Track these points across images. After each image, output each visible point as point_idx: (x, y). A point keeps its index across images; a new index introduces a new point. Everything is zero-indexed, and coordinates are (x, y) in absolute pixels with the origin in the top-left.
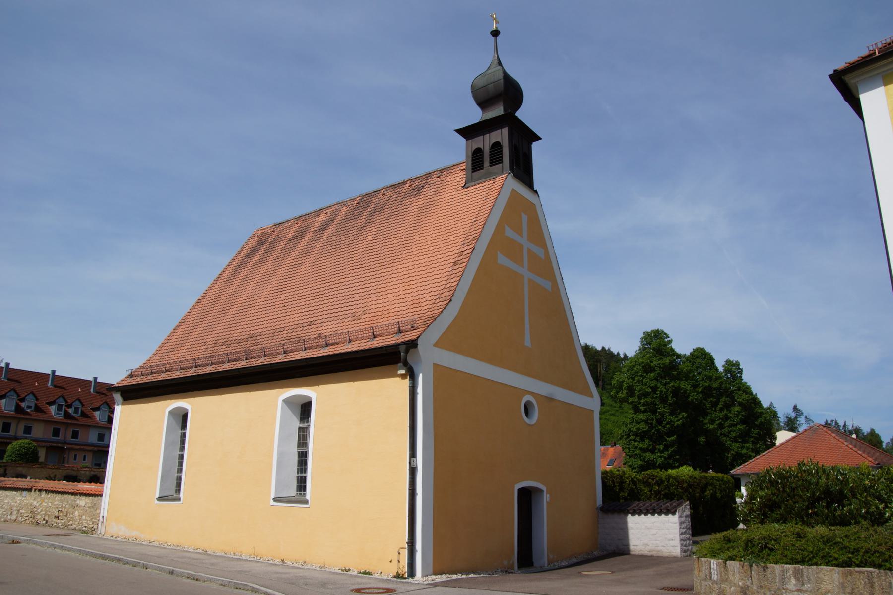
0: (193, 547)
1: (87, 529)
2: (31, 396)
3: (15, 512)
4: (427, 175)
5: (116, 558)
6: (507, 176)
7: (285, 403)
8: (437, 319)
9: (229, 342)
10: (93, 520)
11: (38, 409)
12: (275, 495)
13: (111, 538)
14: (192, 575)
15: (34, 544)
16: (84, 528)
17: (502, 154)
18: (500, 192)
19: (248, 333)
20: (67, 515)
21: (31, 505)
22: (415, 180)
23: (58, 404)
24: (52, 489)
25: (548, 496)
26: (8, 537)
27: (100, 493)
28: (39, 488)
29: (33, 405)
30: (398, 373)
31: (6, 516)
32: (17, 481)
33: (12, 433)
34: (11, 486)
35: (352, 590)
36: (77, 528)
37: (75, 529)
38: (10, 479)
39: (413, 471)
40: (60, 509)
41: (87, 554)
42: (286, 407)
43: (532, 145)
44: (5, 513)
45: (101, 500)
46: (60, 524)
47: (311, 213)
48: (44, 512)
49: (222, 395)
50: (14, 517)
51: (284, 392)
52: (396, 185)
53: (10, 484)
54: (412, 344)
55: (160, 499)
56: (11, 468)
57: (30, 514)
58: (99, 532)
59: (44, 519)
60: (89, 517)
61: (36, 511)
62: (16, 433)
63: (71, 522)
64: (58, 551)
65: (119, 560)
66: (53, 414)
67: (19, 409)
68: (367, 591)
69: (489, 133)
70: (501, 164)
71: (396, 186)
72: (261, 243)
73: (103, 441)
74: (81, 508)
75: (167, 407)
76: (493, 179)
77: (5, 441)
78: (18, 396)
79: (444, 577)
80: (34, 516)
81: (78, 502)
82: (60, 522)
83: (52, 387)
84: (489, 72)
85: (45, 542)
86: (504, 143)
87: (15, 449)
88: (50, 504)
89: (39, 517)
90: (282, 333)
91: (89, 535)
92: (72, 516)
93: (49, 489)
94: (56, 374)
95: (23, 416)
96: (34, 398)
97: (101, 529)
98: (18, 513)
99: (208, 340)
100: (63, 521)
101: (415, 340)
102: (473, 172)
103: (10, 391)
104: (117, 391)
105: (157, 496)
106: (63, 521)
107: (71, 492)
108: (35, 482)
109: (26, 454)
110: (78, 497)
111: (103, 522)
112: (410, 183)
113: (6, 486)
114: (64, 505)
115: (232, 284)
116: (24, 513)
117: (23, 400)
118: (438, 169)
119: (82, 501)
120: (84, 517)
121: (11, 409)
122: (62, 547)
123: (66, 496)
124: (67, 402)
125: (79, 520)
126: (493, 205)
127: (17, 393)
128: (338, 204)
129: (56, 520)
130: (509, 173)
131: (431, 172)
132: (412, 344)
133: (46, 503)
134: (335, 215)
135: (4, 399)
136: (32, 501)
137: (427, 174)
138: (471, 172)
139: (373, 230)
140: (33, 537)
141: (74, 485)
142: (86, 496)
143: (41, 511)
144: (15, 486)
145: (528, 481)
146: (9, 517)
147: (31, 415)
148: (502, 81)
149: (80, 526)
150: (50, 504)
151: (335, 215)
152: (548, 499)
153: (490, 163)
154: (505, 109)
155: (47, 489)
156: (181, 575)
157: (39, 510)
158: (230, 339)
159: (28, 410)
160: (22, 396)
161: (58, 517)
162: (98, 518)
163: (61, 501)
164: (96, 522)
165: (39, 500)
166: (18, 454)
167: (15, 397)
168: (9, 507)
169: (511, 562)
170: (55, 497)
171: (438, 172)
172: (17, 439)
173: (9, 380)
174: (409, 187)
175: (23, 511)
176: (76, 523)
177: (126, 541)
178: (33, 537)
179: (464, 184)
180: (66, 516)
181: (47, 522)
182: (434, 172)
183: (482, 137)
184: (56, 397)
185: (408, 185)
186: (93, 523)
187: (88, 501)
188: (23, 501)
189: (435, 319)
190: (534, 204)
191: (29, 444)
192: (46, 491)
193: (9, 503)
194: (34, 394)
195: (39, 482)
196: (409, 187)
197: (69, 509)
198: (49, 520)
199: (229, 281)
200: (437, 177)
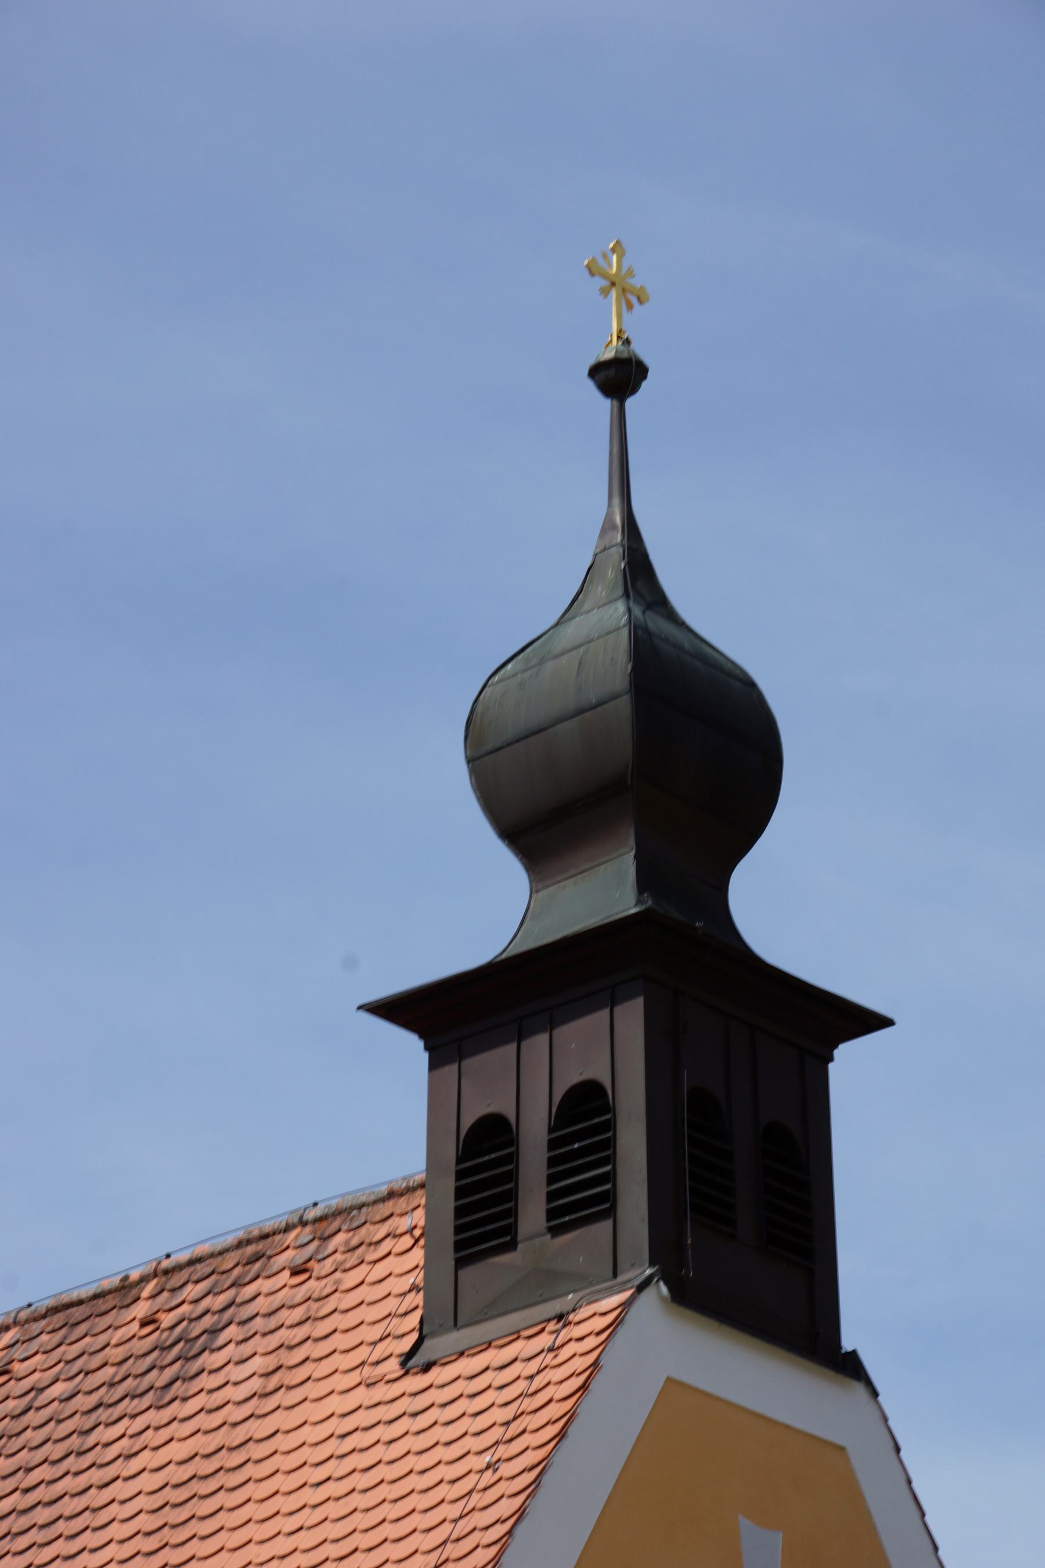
4: (250, 1250)
6: (626, 1305)
17: (611, 1160)
18: (571, 1416)
22: (184, 1275)
43: (834, 1069)
52: (80, 1302)
69: (551, 1026)
70: (606, 1225)
71: (77, 1313)
76: (560, 1317)
84: (573, 631)
102: (460, 1263)
112: (153, 1296)
118: (311, 1215)
126: (521, 1513)
130: (641, 1288)
131: (268, 1227)
137: (249, 1242)
148: (624, 706)
153: (551, 1214)
154: (644, 882)
171: (306, 1233)
174: (144, 1324)
179: (415, 1336)
182: (288, 1229)
185: (141, 1309)
190: (842, 1449)
196: (144, 1324)
200: (295, 1273)
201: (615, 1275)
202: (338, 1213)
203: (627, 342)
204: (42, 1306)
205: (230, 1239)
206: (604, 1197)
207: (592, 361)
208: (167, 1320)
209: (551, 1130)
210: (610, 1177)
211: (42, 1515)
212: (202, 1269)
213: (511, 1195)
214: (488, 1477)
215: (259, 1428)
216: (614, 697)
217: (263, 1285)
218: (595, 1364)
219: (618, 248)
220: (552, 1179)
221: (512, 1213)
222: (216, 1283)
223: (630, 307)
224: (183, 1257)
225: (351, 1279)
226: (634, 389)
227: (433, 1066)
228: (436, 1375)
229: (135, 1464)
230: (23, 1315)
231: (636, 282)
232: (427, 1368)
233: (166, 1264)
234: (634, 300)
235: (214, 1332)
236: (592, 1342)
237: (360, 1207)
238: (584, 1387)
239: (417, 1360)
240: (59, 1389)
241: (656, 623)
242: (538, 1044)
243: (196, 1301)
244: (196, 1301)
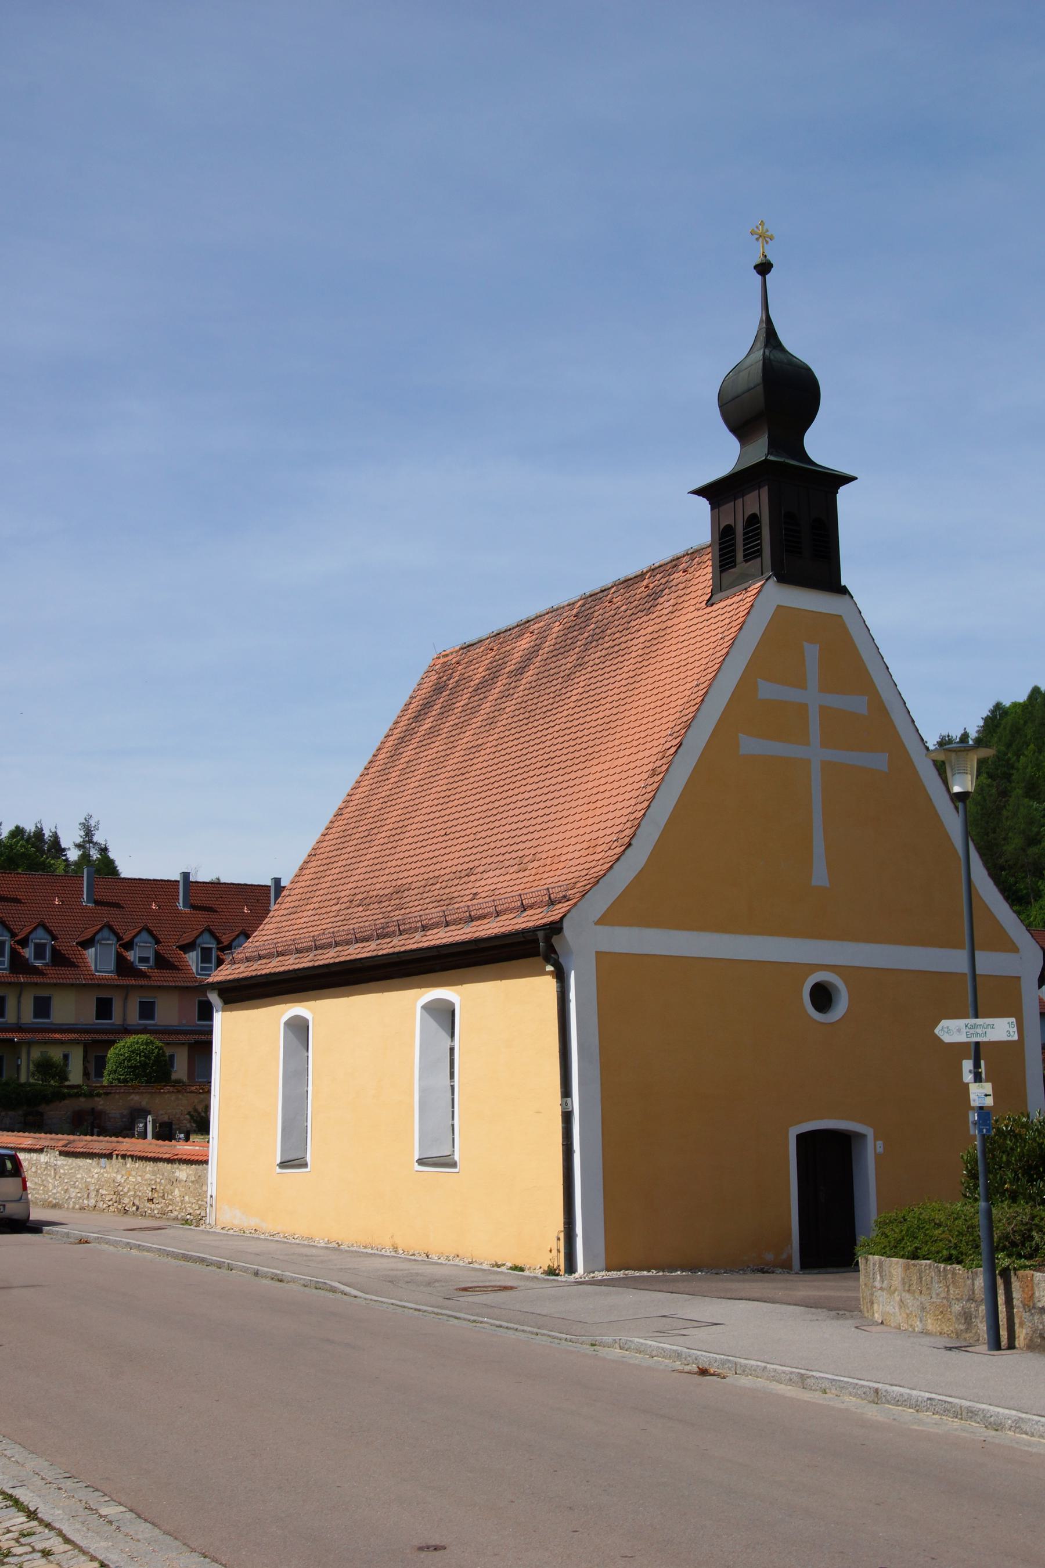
0: (326, 1239)
1: (192, 1217)
2: (145, 935)
3: (93, 1194)
4: (674, 563)
5: (199, 1257)
6: (762, 586)
7: (426, 1011)
8: (601, 881)
9: (367, 901)
10: (200, 1202)
11: (162, 962)
12: (420, 1155)
13: (222, 1231)
14: (276, 1275)
15: (107, 1243)
16: (188, 1217)
18: (744, 622)
19: (394, 883)
20: (164, 1195)
21: (114, 1181)
23: (203, 949)
24: (139, 1154)
25: (879, 1143)
26: (74, 1234)
27: (205, 1158)
28: (122, 1153)
29: (151, 954)
30: (547, 970)
31: (81, 1201)
32: (92, 1141)
33: (117, 1018)
34: (82, 1150)
35: (456, 1289)
36: (179, 1216)
37: (176, 1219)
38: (82, 1137)
39: (567, 1117)
40: (154, 1187)
41: (169, 1254)
42: (425, 1014)
44: (79, 1195)
45: (207, 1170)
46: (156, 1212)
47: (513, 628)
48: (132, 1193)
49: (350, 998)
50: (92, 1202)
51: (423, 994)
52: (631, 579)
53: (81, 1146)
54: (555, 928)
55: (283, 1165)
56: (117, 1096)
57: (115, 1196)
58: (208, 1222)
59: (134, 1204)
60: (194, 1197)
61: (122, 1191)
62: (19, 1018)
63: (170, 1208)
64: (134, 1252)
65: (202, 1260)
66: (194, 971)
67: (123, 967)
68: (478, 1289)
70: (759, 559)
71: (630, 582)
72: (439, 688)
73: (48, 1016)
74: (183, 1184)
75: (283, 1014)
77: (104, 1037)
78: (119, 938)
79: (614, 1274)
80: (120, 1199)
81: (177, 1174)
82: (156, 1208)
83: (187, 910)
85: (119, 1239)
86: (763, 518)
87: (122, 1057)
88: (139, 1179)
89: (126, 1200)
90: (435, 887)
91: (192, 1227)
92: (170, 1197)
93: (136, 1153)
94: (192, 879)
95: (133, 982)
96: (150, 939)
97: (211, 1219)
98: (96, 1195)
99: (343, 894)
100: (159, 1206)
101: (557, 922)
102: (721, 572)
103: (101, 929)
104: (212, 990)
105: (278, 1162)
106: (159, 1206)
107: (165, 1158)
108: (118, 1142)
109: (144, 1065)
110: (176, 1166)
111: (211, 1206)
113: (76, 1150)
114: (158, 1180)
115: (388, 779)
116: (105, 1195)
117: (129, 946)
118: (689, 552)
119: (183, 1172)
120: (187, 1198)
121: (106, 968)
122: (139, 1245)
123: (161, 1165)
124: (219, 941)
125: (180, 1204)
126: (727, 653)
127: (116, 934)
128: (552, 612)
129: (149, 1205)
130: (767, 580)
131: (679, 555)
132: (555, 928)
133: (134, 1176)
134: (543, 636)
135: (91, 948)
136: (115, 1175)
137: (674, 560)
138: (719, 572)
139: (581, 679)
140: (106, 1233)
141: (171, 1146)
142: (187, 1164)
143: (128, 1192)
144: (88, 1150)
145: (825, 1120)
146: (86, 1202)
147: (149, 977)
148: (760, 389)
149: (183, 1214)
150: (139, 1179)
151: (543, 636)
152: (880, 1150)
153: (745, 556)
155: (132, 1153)
156: (265, 1276)
157: (126, 1190)
158: (371, 894)
159: (143, 967)
160: (127, 938)
161: (151, 1200)
162: (205, 1200)
163: (154, 1173)
164: (202, 1205)
165: (124, 1172)
166: (129, 1067)
167: (113, 941)
168: (84, 1185)
169: (784, 1256)
170: (146, 1167)
172: (127, 1031)
173: (97, 903)
175: (104, 1192)
176: (177, 1208)
177: (242, 1234)
178: (106, 1233)
179: (710, 594)
180: (163, 1197)
181: (137, 1209)
182: (684, 556)
183: (732, 503)
184: (196, 933)
185: (645, 582)
186: (199, 1208)
187: (191, 1172)
188: (102, 1174)
189: (598, 881)
190: (841, 616)
191: (147, 1044)
192: (132, 1157)
193: (82, 1178)
194: (150, 932)
195: (123, 1142)
197: (166, 1185)
198: (141, 1206)
199: (384, 771)
201: (762, 575)
202: (697, 551)
203: (765, 256)
204: (622, 579)
205: (669, 559)
206: (758, 551)
207: (754, 264)
208: (651, 586)
209: (744, 530)
210: (760, 544)
211: (616, 648)
212: (662, 569)
213: (734, 551)
214: (722, 641)
215: (669, 623)
216: (758, 385)
217: (676, 575)
218: (752, 605)
219: (762, 223)
220: (745, 545)
221: (735, 556)
222: (664, 574)
223: (767, 242)
224: (657, 565)
225: (697, 574)
226: (769, 271)
227: (712, 509)
228: (715, 607)
229: (640, 633)
230: (617, 583)
231: (769, 234)
232: (712, 605)
233: (653, 567)
234: (768, 240)
235: (662, 591)
236: (753, 597)
237: (703, 549)
238: (748, 613)
239: (710, 603)
240: (624, 608)
241: (778, 355)
242: (739, 501)
243: (659, 580)
244: (659, 580)
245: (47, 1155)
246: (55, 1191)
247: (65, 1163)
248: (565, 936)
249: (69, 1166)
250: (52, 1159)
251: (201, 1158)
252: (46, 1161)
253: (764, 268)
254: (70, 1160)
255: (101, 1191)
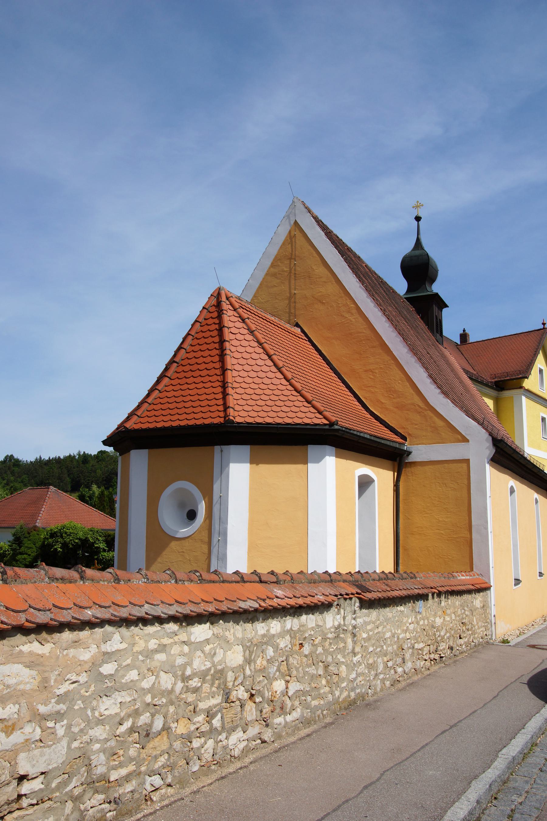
110: (473, 595)
219: (418, 202)
245: (338, 613)
246: (353, 676)
247: (367, 619)
248: (130, 454)
249: (373, 623)
250: (349, 617)
251: (483, 586)
252: (336, 624)
253: (418, 219)
254: (374, 614)
255: (416, 646)
